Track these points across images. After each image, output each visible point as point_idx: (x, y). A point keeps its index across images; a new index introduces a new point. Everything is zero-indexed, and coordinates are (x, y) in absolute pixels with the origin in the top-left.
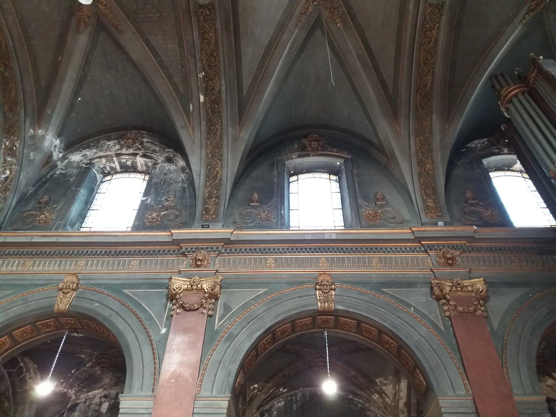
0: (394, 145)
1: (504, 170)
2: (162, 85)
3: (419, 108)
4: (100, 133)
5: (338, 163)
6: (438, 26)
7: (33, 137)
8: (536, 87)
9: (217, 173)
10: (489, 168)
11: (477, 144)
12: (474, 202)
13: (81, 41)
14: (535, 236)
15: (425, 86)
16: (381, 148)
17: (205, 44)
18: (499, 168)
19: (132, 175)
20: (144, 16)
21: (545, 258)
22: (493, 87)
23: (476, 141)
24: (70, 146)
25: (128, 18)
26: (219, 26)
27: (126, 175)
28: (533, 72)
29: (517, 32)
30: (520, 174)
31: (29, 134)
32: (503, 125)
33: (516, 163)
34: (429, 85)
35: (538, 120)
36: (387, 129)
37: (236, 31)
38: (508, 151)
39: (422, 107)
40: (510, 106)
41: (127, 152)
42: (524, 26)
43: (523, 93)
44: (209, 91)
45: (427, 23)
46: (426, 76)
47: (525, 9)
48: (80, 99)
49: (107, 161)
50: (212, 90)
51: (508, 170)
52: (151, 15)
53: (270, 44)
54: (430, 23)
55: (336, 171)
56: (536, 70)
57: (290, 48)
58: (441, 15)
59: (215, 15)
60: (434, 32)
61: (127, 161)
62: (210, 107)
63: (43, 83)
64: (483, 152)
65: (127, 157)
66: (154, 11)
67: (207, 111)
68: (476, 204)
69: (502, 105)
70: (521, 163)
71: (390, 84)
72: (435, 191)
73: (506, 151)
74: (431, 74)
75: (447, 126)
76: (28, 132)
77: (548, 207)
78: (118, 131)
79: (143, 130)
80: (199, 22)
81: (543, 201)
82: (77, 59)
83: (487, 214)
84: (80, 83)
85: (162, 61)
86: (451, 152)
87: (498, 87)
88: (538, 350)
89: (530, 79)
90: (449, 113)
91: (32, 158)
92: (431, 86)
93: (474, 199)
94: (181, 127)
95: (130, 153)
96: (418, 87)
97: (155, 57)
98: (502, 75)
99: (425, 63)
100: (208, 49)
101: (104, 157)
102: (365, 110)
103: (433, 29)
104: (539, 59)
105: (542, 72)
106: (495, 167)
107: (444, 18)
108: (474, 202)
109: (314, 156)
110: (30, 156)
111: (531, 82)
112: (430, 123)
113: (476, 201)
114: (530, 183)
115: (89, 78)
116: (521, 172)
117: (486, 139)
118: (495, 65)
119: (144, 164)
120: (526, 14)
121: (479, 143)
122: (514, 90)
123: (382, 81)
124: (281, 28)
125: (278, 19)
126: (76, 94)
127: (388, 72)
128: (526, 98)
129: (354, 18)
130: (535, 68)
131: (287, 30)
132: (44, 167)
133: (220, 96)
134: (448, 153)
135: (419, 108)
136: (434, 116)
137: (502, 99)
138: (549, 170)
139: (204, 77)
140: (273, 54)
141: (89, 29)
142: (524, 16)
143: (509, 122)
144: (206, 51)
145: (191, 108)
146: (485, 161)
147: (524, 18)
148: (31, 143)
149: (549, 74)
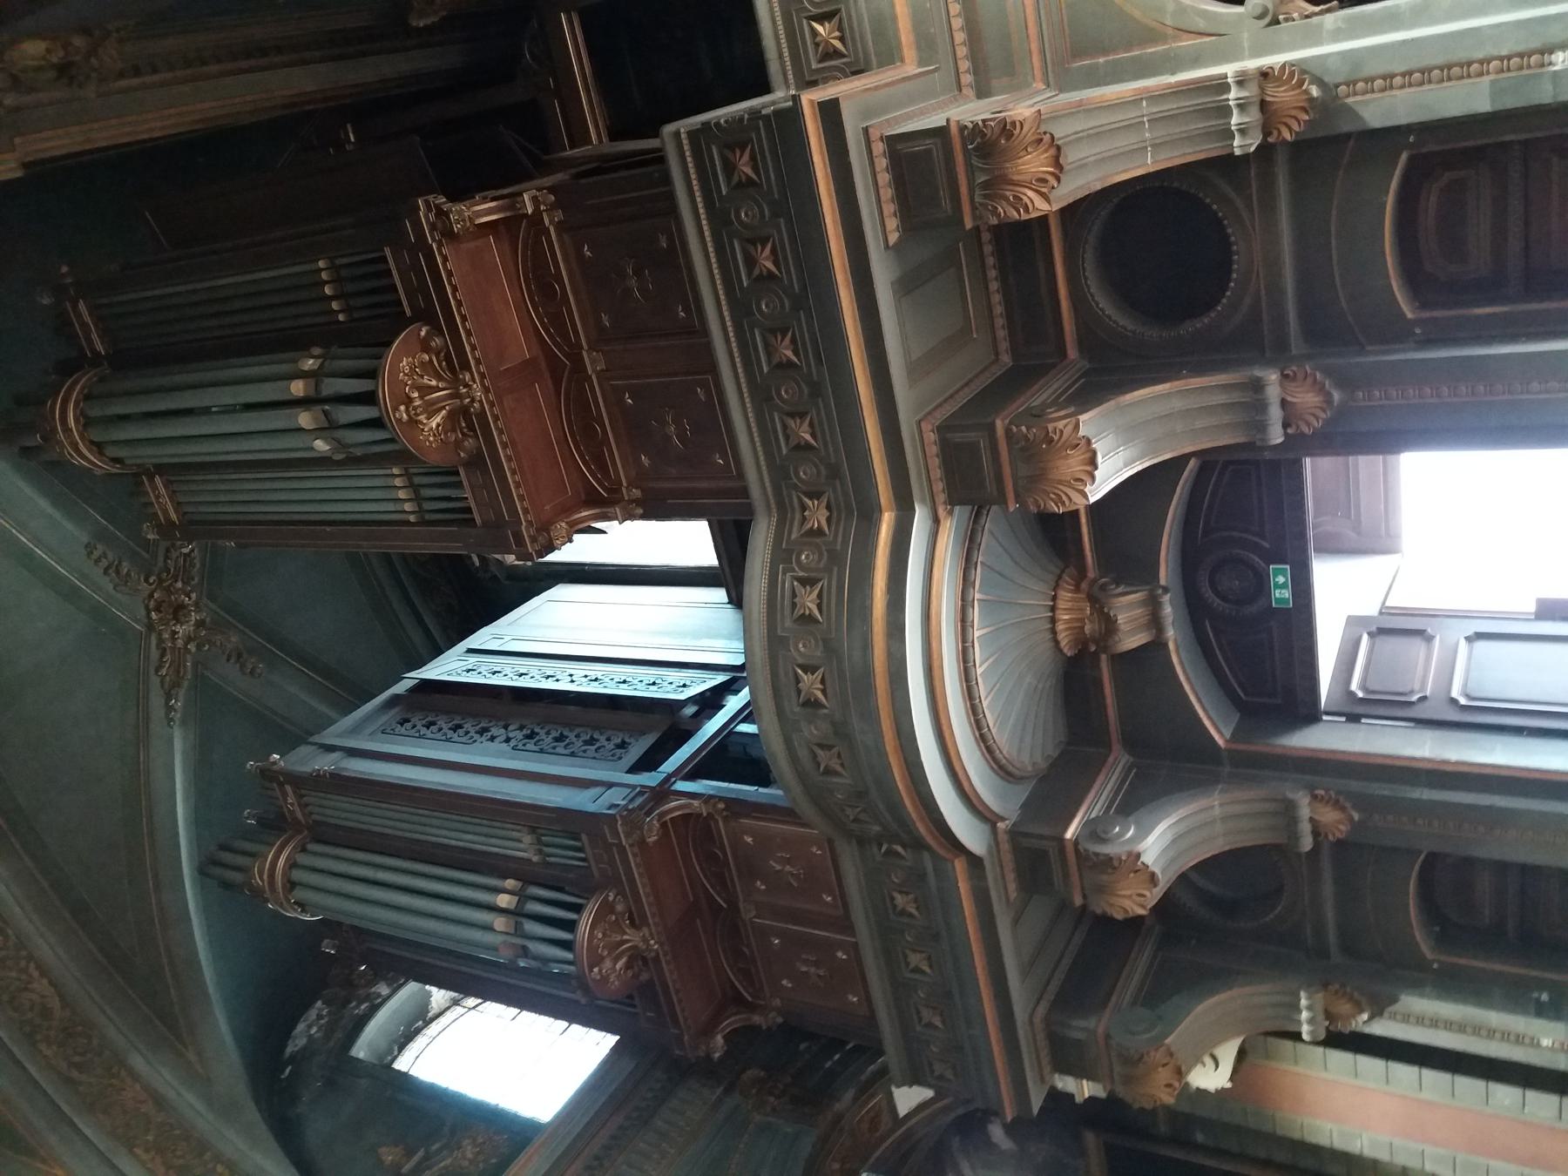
1: (418, 1031)
3: (75, 1074)
8: (315, 817)
10: (381, 1058)
11: (307, 1029)
12: (416, 1158)
14: (603, 1099)
15: (46, 1013)
18: (405, 1038)
21: (660, 1123)
22: (226, 885)
23: (301, 1027)
28: (285, 795)
29: (178, 745)
30: (458, 1010)
32: (326, 941)
33: (429, 995)
34: (55, 1003)
35: (382, 876)
38: (389, 985)
39: (79, 1067)
40: (299, 894)
42: (184, 723)
43: (304, 850)
46: (26, 989)
47: (156, 699)
51: (428, 1023)
56: (288, 788)
64: (339, 1035)
68: (426, 1158)
69: (281, 906)
70: (440, 986)
73: (384, 990)
74: (36, 974)
75: (192, 1056)
77: (572, 1019)
81: (514, 1011)
83: (470, 1156)
86: (257, 1102)
87: (237, 877)
89: (292, 812)
90: (166, 1016)
92: (62, 997)
93: (410, 1153)
96: (27, 1029)
98: (224, 847)
104: (274, 763)
105: (301, 782)
106: (395, 1041)
108: (416, 1158)
111: (299, 815)
112: (138, 1087)
113: (421, 1153)
114: (494, 1009)
116: (456, 1003)
117: (319, 1004)
118: (190, 842)
120: (168, 699)
121: (310, 1027)
122: (278, 858)
128: (315, 854)
130: (281, 785)
134: (252, 1113)
135: (75, 1074)
136: (137, 1062)
137: (268, 894)
138: (496, 949)
142: (167, 703)
143: (330, 926)
146: (360, 1051)
147: (169, 709)
149: (318, 775)
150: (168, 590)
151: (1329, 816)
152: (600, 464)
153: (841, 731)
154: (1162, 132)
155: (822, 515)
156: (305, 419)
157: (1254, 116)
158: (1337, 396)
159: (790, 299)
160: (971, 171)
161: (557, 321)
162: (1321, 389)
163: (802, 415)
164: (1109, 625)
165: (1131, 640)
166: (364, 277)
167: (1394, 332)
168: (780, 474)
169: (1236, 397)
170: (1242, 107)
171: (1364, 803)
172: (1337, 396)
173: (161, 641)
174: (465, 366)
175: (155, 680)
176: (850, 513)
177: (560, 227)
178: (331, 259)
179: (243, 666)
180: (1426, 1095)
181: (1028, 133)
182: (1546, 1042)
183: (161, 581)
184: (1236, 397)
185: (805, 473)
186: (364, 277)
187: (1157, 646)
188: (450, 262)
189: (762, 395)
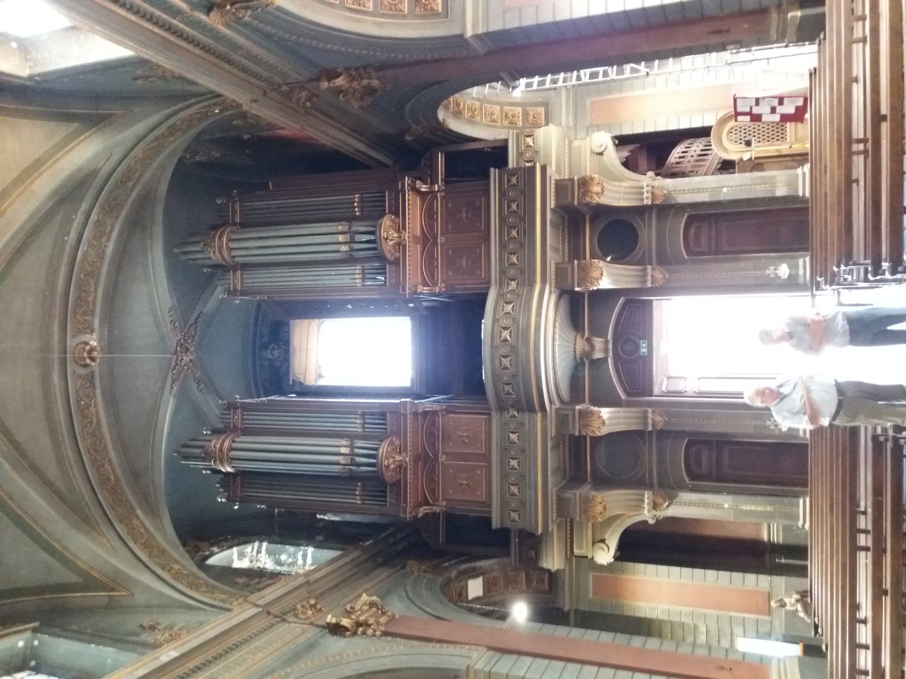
0: (114, 561)
6: (95, 402)
16: (90, 583)
36: (92, 546)
42: (174, 397)
43: (234, 441)
47: (169, 381)
54: (84, 398)
58: (94, 388)
60: (92, 409)
71: (61, 485)
72: (213, 587)
88: (756, 158)
98: (184, 446)
99: (96, 451)
103: (90, 405)
107: (98, 391)
127: (52, 471)
132: (109, 116)
147: (172, 388)
150: (186, 341)
151: (658, 419)
152: (432, 275)
153: (514, 349)
154: (626, 196)
155: (515, 286)
156: (341, 238)
157: (650, 195)
158: (667, 276)
159: (520, 220)
160: (579, 189)
161: (431, 227)
162: (662, 273)
163: (515, 254)
164: (592, 346)
165: (598, 355)
166: (375, 201)
167: (679, 261)
168: (503, 272)
169: (638, 273)
170: (647, 192)
171: (668, 414)
172: (667, 276)
173: (177, 359)
174: (404, 228)
175: (170, 374)
176: (524, 284)
177: (442, 198)
178: (362, 194)
179: (198, 386)
180: (683, 581)
181: (597, 181)
182: (726, 506)
183: (184, 336)
184: (638, 273)
185: (512, 272)
186: (372, 201)
187: (605, 360)
188: (409, 196)
189: (503, 246)
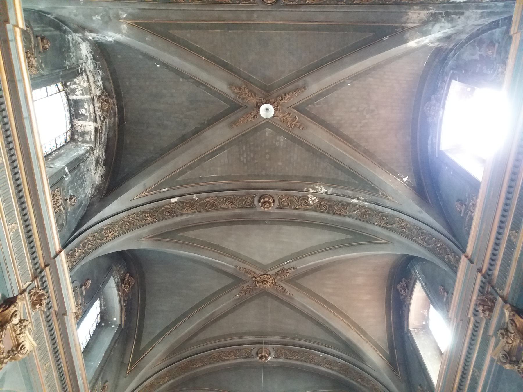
0: (147, 366)
2: (181, 159)
4: (113, 73)
5: (115, 319)
7: (118, 17)
9: (107, 237)
13: (220, 83)
16: (138, 353)
17: (222, 200)
19: (68, 113)
20: (244, 149)
24: (101, 50)
25: (243, 135)
26: (237, 211)
27: (67, 108)
31: (120, 12)
37: (231, 223)
41: (97, 109)
44: (181, 205)
45: (239, 352)
48: (158, 66)
49: (85, 88)
50: (182, 207)
52: (245, 156)
53: (223, 248)
55: (105, 317)
57: (218, 263)
59: (246, 208)
60: (233, 357)
61: (86, 109)
62: (167, 208)
63: (177, 33)
65: (92, 110)
66: (248, 159)
67: (163, 206)
76: (122, 10)
78: (115, 90)
79: (119, 118)
80: (241, 196)
82: (203, 76)
84: (178, 72)
85: (205, 161)
91: (94, 18)
94: (145, 184)
95: (97, 112)
97: (208, 154)
99: (211, 358)
100: (218, 202)
101: (90, 85)
102: (168, 328)
109: (119, 295)
110: (95, 16)
115: (181, 80)
119: (86, 130)
123: (196, 334)
124: (235, 256)
125: (242, 253)
126: (164, 65)
127: (201, 336)
129: (241, 305)
131: (233, 260)
133: (178, 215)
139: (194, 199)
140: (214, 251)
141: (233, 96)
144: (216, 200)
145: (164, 190)
148: (111, 16)
